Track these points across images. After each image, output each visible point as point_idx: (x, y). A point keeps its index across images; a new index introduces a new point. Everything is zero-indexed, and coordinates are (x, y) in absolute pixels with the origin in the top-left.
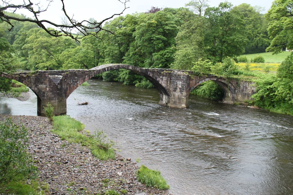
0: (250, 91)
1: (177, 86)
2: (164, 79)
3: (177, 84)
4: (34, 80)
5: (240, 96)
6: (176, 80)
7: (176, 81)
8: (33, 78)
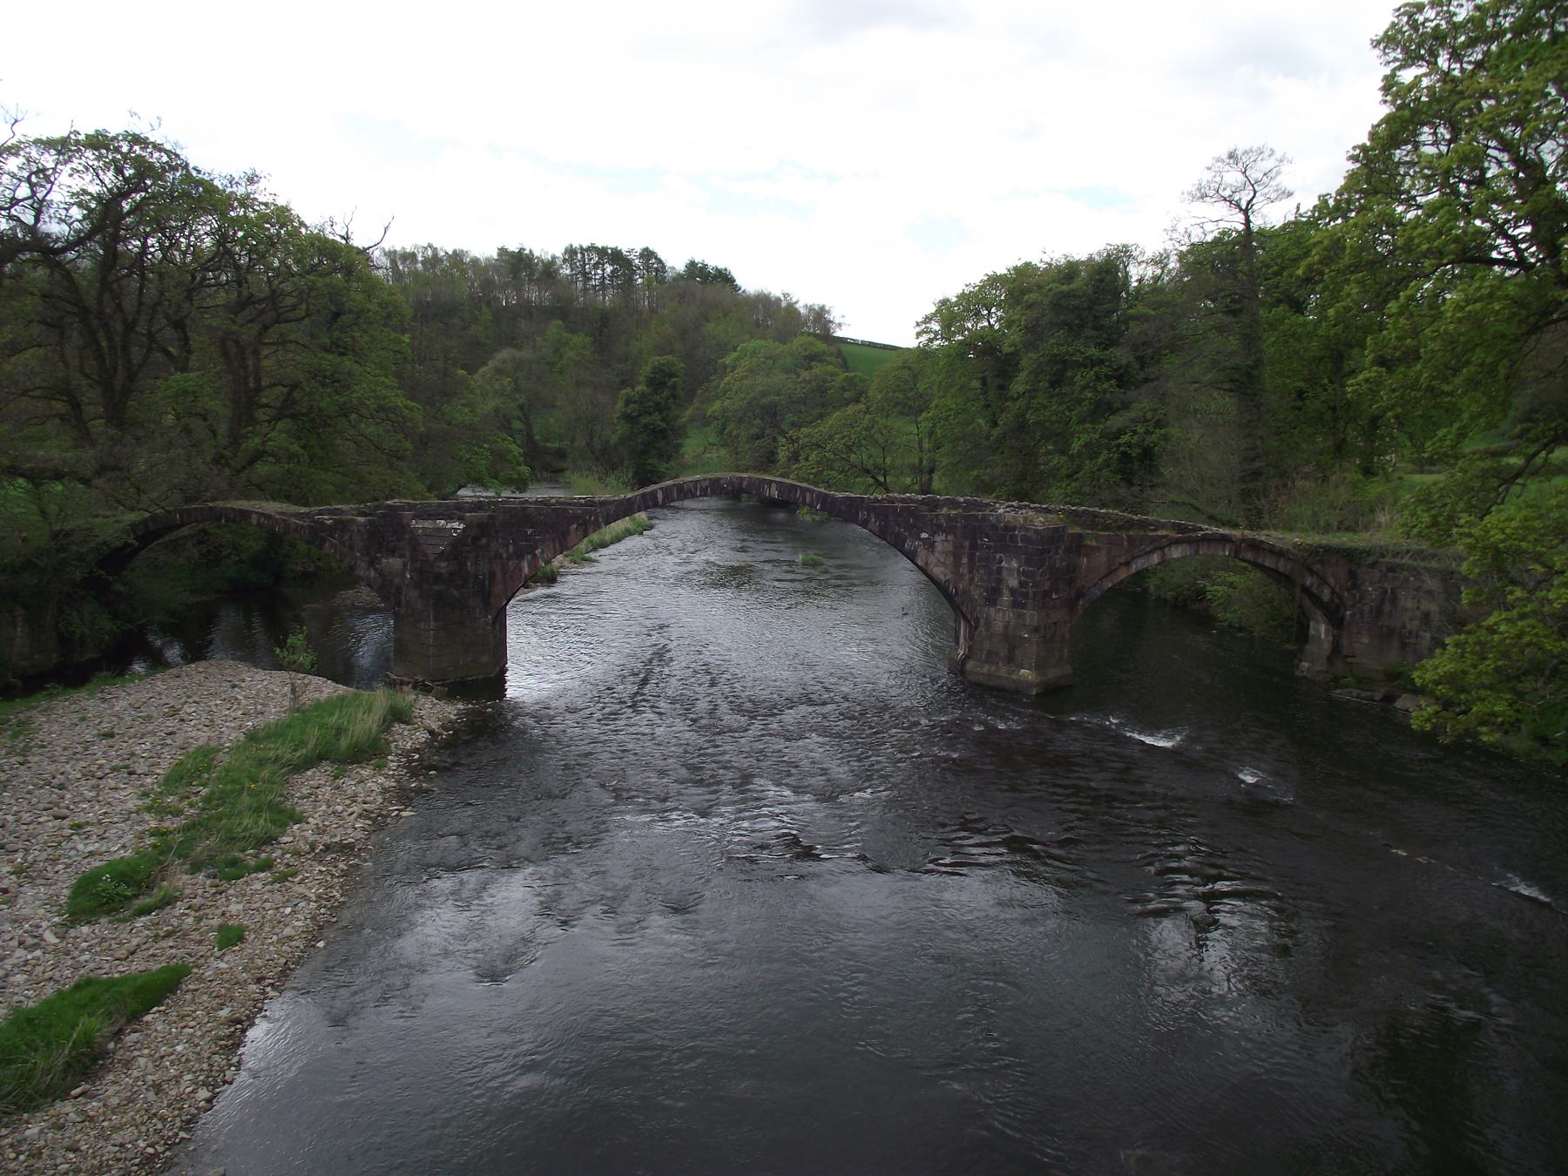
0: (1411, 619)
1: (1000, 581)
2: (939, 547)
3: (1000, 570)
4: (365, 536)
5: (1366, 640)
6: (996, 552)
7: (998, 556)
8: (359, 531)
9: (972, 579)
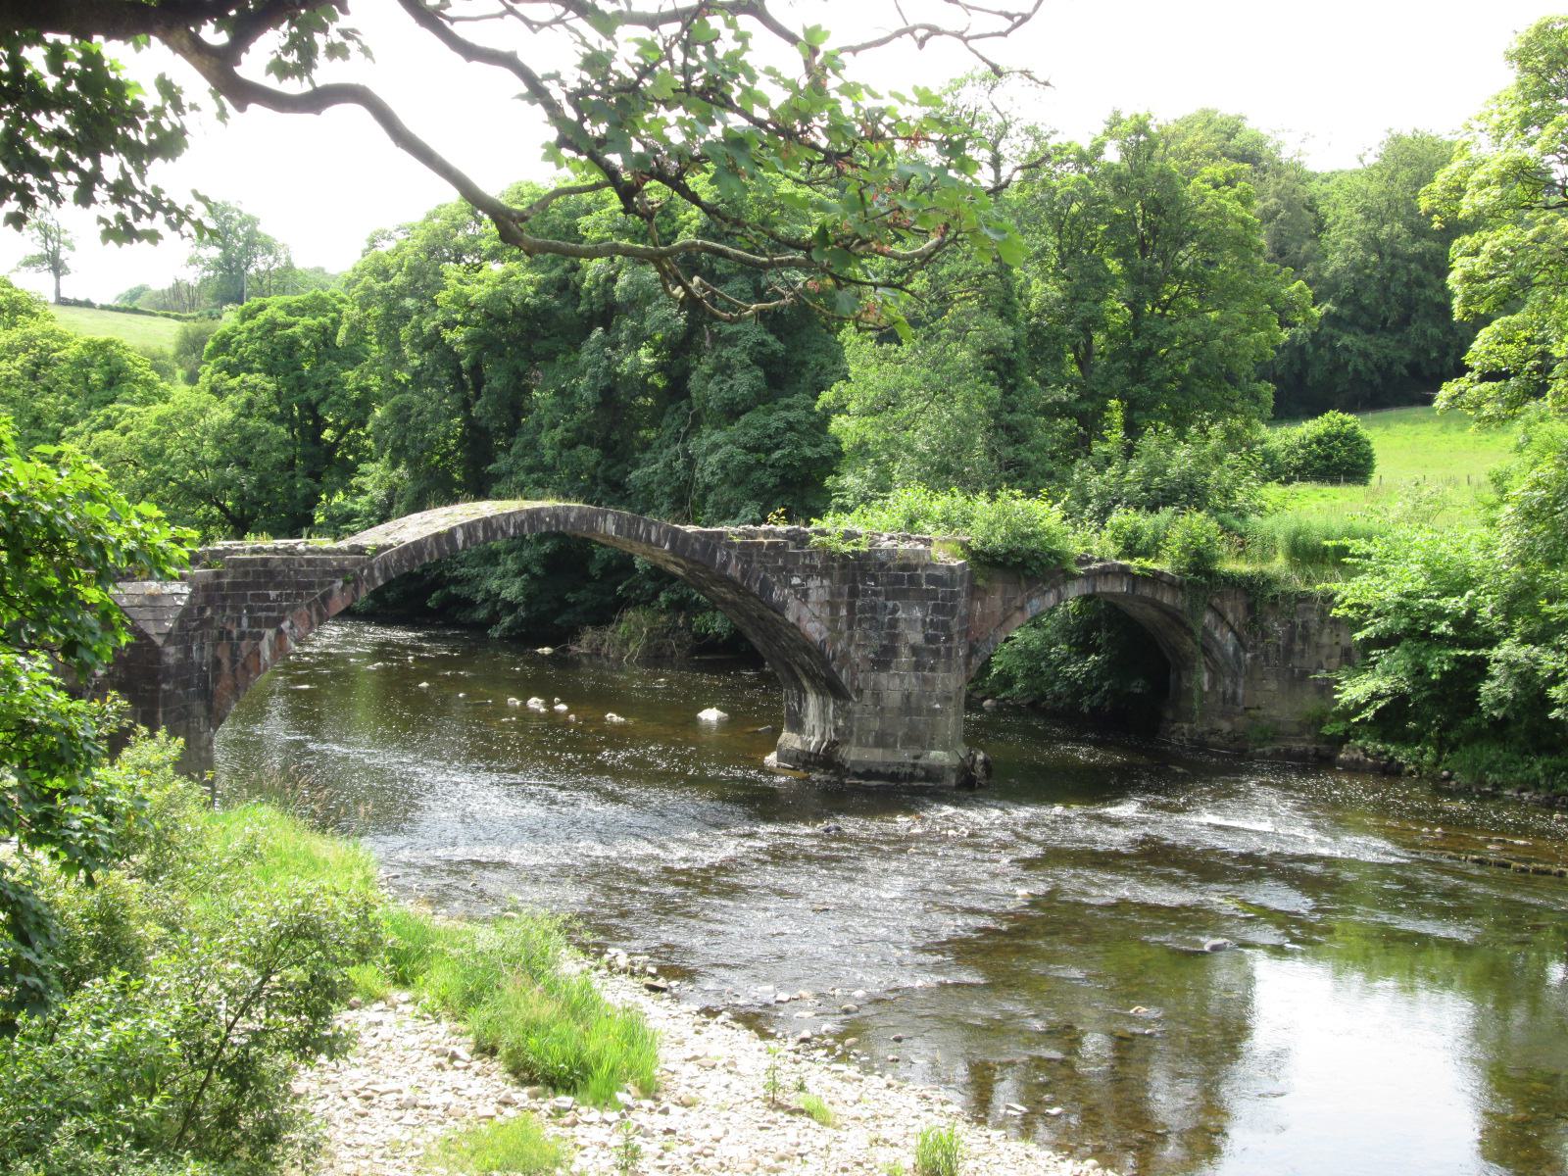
1: (894, 637)
2: (813, 596)
7: (890, 604)
9: (851, 637)
